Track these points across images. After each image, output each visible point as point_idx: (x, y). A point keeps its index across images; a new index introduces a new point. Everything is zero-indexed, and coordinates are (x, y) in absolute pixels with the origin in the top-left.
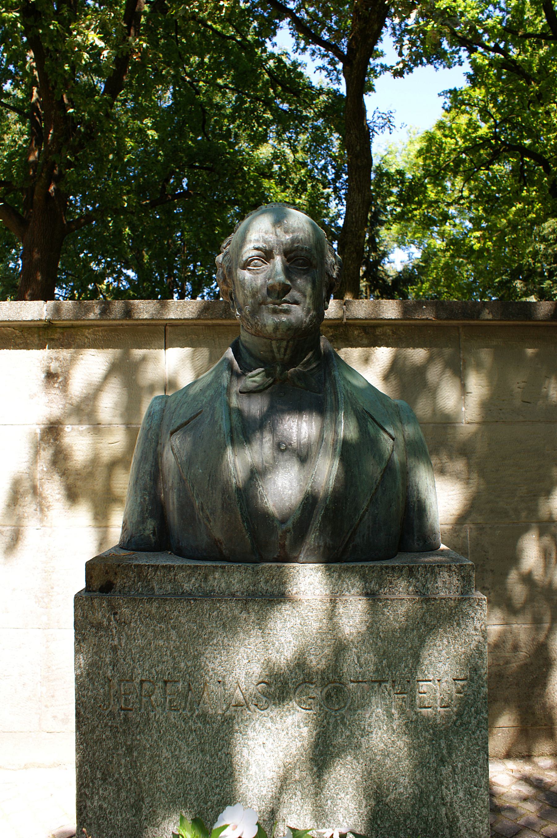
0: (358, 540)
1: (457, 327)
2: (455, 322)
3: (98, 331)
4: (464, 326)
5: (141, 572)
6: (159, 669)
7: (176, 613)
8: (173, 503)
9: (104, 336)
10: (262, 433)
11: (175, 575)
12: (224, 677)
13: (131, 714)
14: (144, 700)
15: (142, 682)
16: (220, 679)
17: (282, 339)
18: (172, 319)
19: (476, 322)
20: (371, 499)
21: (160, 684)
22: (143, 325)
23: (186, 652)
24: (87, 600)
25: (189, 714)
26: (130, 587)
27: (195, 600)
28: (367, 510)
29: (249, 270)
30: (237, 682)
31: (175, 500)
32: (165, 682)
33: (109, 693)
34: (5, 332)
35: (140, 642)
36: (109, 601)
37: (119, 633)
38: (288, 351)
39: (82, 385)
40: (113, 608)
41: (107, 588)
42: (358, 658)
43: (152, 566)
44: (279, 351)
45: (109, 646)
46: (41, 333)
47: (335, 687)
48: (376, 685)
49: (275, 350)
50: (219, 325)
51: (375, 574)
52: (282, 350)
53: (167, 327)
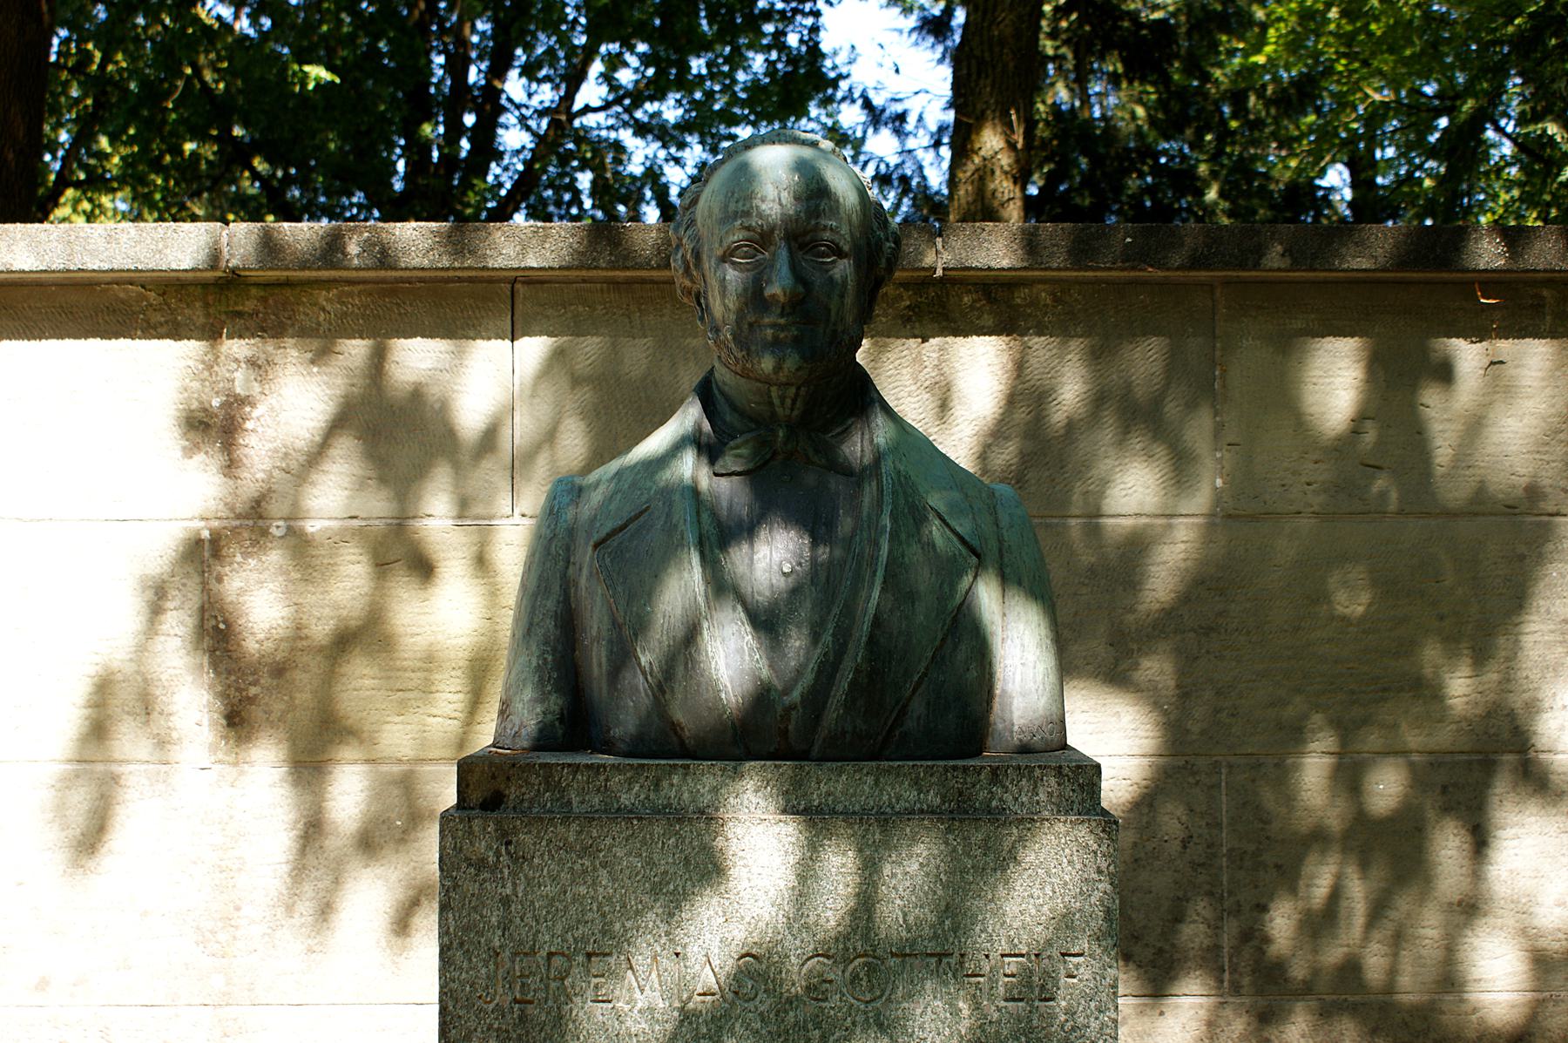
0: (910, 724)
1: (1210, 287)
2: (1203, 275)
3: (351, 295)
4: (1227, 283)
5: (551, 775)
6: (578, 934)
7: (608, 841)
8: (600, 665)
9: (366, 307)
10: (752, 545)
11: (607, 780)
12: (685, 947)
13: (530, 1009)
14: (553, 985)
15: (550, 955)
16: (679, 949)
17: (788, 384)
18: (532, 268)
19: (1254, 273)
20: (933, 657)
21: (580, 958)
22: (460, 280)
23: (624, 906)
24: (462, 820)
25: (627, 1008)
26: (531, 801)
27: (640, 819)
28: (925, 674)
29: (734, 263)
30: (706, 955)
31: (604, 660)
32: (589, 956)
33: (496, 976)
34: (122, 295)
35: (548, 890)
36: (498, 823)
37: (513, 874)
38: (798, 404)
39: (312, 424)
40: (505, 834)
41: (493, 803)
42: (905, 915)
43: (570, 765)
44: (783, 404)
45: (498, 897)
46: (210, 299)
47: (865, 964)
48: (933, 960)
49: (776, 401)
50: (643, 281)
51: (934, 779)
52: (788, 402)
53: (518, 286)
